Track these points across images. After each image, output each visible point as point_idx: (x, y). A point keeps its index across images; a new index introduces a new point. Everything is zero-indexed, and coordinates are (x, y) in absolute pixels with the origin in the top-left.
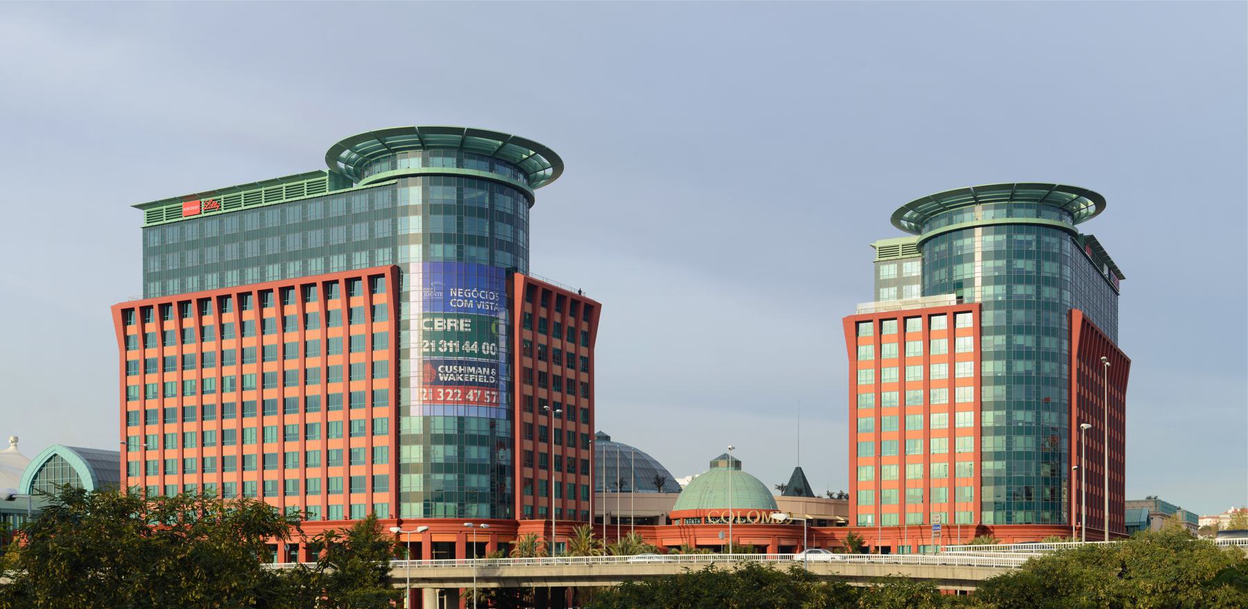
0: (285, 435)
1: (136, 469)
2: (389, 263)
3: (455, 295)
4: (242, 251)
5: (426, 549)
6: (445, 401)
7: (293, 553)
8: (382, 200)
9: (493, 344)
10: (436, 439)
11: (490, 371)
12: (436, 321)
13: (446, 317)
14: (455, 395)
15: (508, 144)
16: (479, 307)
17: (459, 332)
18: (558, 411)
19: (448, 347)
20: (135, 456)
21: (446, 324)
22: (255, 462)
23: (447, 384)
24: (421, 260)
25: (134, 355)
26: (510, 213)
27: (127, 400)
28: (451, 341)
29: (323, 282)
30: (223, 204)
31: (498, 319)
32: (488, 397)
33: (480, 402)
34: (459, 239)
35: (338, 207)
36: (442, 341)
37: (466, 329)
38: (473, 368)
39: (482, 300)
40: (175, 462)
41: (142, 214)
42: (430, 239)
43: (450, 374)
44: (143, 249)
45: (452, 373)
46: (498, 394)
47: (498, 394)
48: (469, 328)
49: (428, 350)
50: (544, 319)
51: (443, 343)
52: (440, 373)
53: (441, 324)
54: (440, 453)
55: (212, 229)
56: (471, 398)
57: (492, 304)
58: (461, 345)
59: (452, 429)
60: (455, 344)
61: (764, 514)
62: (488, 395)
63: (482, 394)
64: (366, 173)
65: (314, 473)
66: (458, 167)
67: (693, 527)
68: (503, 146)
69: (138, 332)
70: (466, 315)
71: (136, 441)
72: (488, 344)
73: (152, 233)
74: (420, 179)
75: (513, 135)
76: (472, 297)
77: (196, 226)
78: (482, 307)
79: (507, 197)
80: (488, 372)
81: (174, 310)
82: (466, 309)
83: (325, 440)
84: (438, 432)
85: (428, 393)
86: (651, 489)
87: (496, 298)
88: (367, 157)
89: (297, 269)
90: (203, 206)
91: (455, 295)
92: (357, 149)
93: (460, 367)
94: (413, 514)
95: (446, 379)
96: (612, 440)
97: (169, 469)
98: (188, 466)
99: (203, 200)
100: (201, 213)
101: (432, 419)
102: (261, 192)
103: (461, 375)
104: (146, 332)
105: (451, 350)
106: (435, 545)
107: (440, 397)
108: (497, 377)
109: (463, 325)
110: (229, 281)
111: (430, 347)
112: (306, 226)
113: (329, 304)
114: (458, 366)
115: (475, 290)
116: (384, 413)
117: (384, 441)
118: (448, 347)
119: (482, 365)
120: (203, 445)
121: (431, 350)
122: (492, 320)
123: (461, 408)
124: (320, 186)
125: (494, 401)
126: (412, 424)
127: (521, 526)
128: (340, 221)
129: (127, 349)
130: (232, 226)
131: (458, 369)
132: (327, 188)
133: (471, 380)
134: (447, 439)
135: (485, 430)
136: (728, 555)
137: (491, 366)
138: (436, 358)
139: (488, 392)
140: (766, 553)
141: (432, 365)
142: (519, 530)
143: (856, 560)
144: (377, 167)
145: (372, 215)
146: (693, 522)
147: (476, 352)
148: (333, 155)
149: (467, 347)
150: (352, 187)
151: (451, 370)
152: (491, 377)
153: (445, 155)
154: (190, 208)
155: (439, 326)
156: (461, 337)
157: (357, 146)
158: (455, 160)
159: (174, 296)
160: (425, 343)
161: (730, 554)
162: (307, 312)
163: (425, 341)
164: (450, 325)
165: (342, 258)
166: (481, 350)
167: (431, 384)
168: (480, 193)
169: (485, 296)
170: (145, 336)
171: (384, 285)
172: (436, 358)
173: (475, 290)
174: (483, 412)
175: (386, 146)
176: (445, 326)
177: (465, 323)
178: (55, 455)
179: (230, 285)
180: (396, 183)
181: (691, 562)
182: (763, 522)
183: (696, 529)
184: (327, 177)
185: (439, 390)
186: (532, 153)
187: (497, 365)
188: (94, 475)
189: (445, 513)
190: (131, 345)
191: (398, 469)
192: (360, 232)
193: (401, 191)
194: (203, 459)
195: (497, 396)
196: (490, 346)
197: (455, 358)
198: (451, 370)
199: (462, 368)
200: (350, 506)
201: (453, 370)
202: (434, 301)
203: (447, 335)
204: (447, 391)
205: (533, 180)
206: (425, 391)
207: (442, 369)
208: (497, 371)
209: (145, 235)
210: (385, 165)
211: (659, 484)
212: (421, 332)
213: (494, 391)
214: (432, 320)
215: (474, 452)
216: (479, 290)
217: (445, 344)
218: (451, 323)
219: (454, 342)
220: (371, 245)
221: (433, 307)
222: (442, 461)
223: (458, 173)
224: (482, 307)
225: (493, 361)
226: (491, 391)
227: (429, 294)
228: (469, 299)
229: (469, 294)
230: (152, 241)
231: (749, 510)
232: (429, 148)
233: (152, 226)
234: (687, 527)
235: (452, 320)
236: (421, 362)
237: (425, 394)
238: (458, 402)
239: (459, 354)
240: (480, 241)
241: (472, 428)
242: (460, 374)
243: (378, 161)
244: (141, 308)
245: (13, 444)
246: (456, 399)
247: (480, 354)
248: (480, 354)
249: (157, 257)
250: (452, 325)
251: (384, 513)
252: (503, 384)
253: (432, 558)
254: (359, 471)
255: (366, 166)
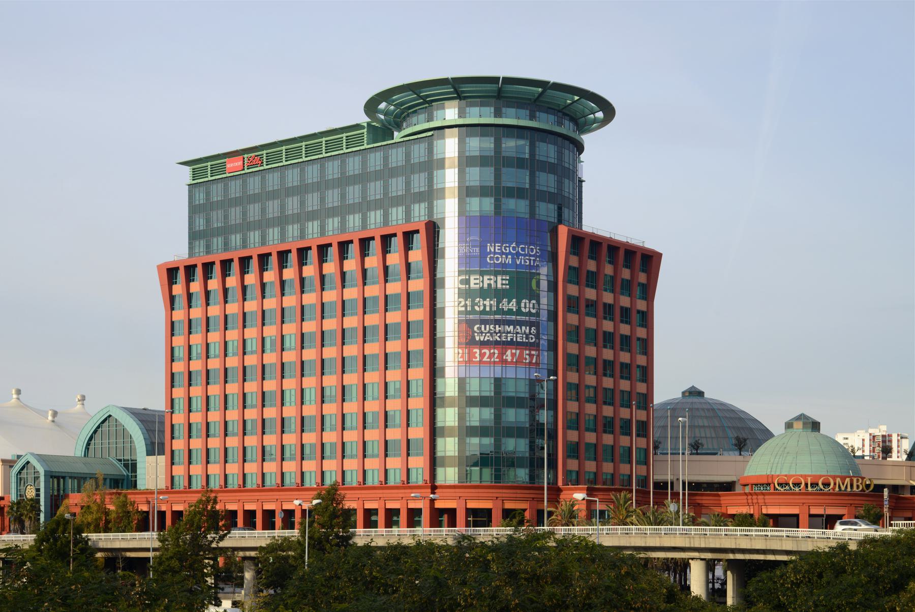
0: (323, 396)
1: (181, 431)
2: (425, 219)
3: (493, 250)
4: (244, 213)
5: (461, 517)
6: (481, 362)
7: (445, 518)
8: (419, 152)
9: (534, 302)
10: (472, 401)
11: (530, 330)
12: (472, 278)
13: (482, 274)
14: (493, 354)
15: (549, 91)
16: (518, 263)
17: (496, 289)
18: (552, 377)
19: (485, 306)
20: (179, 418)
21: (483, 282)
22: (293, 424)
23: (483, 344)
24: (457, 214)
25: (179, 315)
26: (553, 162)
27: (172, 360)
28: (488, 300)
29: (404, 233)
30: (265, 160)
31: (539, 274)
32: (527, 357)
33: (519, 362)
34: (498, 192)
35: (375, 161)
36: (478, 299)
37: (504, 286)
38: (512, 327)
39: (522, 255)
40: (217, 424)
41: (188, 170)
42: (466, 192)
43: (486, 333)
44: (189, 206)
45: (488, 332)
46: (539, 353)
47: (539, 353)
48: (506, 284)
49: (463, 309)
50: (592, 272)
51: (479, 302)
52: (475, 332)
53: (477, 281)
54: (476, 416)
55: (254, 185)
56: (509, 359)
57: (532, 258)
58: (498, 303)
59: (488, 390)
60: (492, 302)
61: (838, 480)
62: (527, 354)
63: (521, 354)
64: (404, 124)
65: (351, 436)
66: (495, 117)
67: (763, 494)
68: (543, 93)
69: (295, 276)
70: (504, 271)
71: (180, 405)
72: (527, 301)
73: (197, 190)
74: (456, 130)
75: (552, 82)
76: (510, 253)
77: (239, 182)
78: (521, 261)
79: (549, 145)
80: (527, 331)
81: (313, 255)
82: (504, 265)
83: (300, 406)
84: (473, 394)
85: (463, 353)
86: (731, 450)
87: (536, 252)
88: (404, 108)
89: (336, 225)
90: (246, 161)
91: (493, 250)
92: (394, 101)
93: (497, 326)
94: (448, 478)
95: (482, 339)
96: (706, 396)
97: (212, 431)
98: (230, 428)
99: (246, 156)
100: (244, 170)
101: (468, 380)
102: (342, 138)
103: (499, 335)
104: (265, 281)
105: (488, 309)
106: (470, 512)
107: (476, 358)
108: (537, 336)
109: (501, 282)
110: (310, 231)
111: (466, 306)
112: (344, 181)
113: (324, 268)
114: (495, 325)
115: (514, 245)
116: (419, 374)
117: (419, 404)
118: (485, 306)
119: (521, 323)
120: (244, 407)
121: (466, 308)
122: (532, 275)
123: (498, 369)
124: (359, 140)
125: (534, 361)
126: (449, 386)
127: (564, 492)
128: (377, 175)
129: (172, 309)
130: (273, 181)
131: (495, 328)
132: (365, 142)
133: (509, 339)
134: (482, 402)
135: (523, 390)
136: (678, 527)
137: (531, 324)
138: (472, 317)
139: (527, 352)
140: (456, 527)
141: (467, 324)
142: (561, 496)
143: (776, 534)
144: (414, 119)
145: (409, 169)
146: (762, 488)
147: (514, 310)
148: (371, 106)
149: (505, 305)
150: (393, 139)
151: (488, 329)
152: (531, 336)
153: (482, 105)
154: (233, 165)
155: (475, 284)
156: (499, 294)
157: (394, 97)
158: (492, 109)
159: (217, 257)
160: (460, 302)
161: (681, 527)
162: (324, 273)
163: (461, 300)
164: (486, 282)
165: (379, 213)
166: (520, 307)
167: (467, 344)
168: (521, 142)
169: (525, 251)
170: (263, 286)
171: (420, 241)
172: (472, 317)
173: (514, 245)
174: (522, 373)
175: (421, 97)
176: (481, 283)
177: (502, 279)
178: (110, 416)
179: (331, 233)
180: (432, 135)
181: (645, 534)
182: (837, 489)
183: (767, 497)
184: (365, 130)
185: (475, 350)
186: (576, 98)
187: (538, 323)
188: (147, 436)
189: (481, 478)
190: (176, 305)
191: (434, 432)
192: (397, 186)
193: (437, 143)
194: (364, 414)
195: (538, 356)
196: (530, 303)
197: (492, 317)
198: (488, 329)
199: (499, 327)
200: (408, 470)
201: (490, 329)
202: (470, 257)
203: (484, 293)
204: (483, 351)
205: (584, 126)
206: (460, 351)
207: (478, 328)
208: (538, 330)
209: (190, 192)
210: (422, 117)
211: (740, 445)
212: (457, 290)
213: (534, 350)
214: (467, 277)
215: (512, 416)
216: (518, 244)
217: (482, 303)
218: (487, 280)
219: (491, 300)
220: (408, 199)
221: (467, 264)
222: (477, 424)
223: (496, 123)
224: (521, 261)
225: (533, 319)
226: (530, 350)
227: (465, 250)
228: (507, 255)
229: (508, 249)
230: (197, 198)
231: (821, 476)
232: (465, 98)
233: (271, 168)
234: (756, 494)
235: (489, 277)
236: (456, 321)
237: (460, 355)
238: (495, 363)
239: (496, 313)
240: (518, 193)
241: (510, 390)
242: (497, 333)
243: (415, 112)
244: (185, 267)
245: (80, 403)
246: (493, 360)
247: (519, 312)
248: (519, 312)
249: (201, 215)
250: (488, 282)
251: (353, 479)
252: (544, 343)
253: (467, 526)
254: (395, 434)
255: (404, 117)
